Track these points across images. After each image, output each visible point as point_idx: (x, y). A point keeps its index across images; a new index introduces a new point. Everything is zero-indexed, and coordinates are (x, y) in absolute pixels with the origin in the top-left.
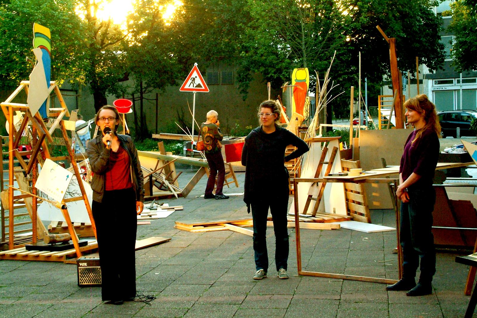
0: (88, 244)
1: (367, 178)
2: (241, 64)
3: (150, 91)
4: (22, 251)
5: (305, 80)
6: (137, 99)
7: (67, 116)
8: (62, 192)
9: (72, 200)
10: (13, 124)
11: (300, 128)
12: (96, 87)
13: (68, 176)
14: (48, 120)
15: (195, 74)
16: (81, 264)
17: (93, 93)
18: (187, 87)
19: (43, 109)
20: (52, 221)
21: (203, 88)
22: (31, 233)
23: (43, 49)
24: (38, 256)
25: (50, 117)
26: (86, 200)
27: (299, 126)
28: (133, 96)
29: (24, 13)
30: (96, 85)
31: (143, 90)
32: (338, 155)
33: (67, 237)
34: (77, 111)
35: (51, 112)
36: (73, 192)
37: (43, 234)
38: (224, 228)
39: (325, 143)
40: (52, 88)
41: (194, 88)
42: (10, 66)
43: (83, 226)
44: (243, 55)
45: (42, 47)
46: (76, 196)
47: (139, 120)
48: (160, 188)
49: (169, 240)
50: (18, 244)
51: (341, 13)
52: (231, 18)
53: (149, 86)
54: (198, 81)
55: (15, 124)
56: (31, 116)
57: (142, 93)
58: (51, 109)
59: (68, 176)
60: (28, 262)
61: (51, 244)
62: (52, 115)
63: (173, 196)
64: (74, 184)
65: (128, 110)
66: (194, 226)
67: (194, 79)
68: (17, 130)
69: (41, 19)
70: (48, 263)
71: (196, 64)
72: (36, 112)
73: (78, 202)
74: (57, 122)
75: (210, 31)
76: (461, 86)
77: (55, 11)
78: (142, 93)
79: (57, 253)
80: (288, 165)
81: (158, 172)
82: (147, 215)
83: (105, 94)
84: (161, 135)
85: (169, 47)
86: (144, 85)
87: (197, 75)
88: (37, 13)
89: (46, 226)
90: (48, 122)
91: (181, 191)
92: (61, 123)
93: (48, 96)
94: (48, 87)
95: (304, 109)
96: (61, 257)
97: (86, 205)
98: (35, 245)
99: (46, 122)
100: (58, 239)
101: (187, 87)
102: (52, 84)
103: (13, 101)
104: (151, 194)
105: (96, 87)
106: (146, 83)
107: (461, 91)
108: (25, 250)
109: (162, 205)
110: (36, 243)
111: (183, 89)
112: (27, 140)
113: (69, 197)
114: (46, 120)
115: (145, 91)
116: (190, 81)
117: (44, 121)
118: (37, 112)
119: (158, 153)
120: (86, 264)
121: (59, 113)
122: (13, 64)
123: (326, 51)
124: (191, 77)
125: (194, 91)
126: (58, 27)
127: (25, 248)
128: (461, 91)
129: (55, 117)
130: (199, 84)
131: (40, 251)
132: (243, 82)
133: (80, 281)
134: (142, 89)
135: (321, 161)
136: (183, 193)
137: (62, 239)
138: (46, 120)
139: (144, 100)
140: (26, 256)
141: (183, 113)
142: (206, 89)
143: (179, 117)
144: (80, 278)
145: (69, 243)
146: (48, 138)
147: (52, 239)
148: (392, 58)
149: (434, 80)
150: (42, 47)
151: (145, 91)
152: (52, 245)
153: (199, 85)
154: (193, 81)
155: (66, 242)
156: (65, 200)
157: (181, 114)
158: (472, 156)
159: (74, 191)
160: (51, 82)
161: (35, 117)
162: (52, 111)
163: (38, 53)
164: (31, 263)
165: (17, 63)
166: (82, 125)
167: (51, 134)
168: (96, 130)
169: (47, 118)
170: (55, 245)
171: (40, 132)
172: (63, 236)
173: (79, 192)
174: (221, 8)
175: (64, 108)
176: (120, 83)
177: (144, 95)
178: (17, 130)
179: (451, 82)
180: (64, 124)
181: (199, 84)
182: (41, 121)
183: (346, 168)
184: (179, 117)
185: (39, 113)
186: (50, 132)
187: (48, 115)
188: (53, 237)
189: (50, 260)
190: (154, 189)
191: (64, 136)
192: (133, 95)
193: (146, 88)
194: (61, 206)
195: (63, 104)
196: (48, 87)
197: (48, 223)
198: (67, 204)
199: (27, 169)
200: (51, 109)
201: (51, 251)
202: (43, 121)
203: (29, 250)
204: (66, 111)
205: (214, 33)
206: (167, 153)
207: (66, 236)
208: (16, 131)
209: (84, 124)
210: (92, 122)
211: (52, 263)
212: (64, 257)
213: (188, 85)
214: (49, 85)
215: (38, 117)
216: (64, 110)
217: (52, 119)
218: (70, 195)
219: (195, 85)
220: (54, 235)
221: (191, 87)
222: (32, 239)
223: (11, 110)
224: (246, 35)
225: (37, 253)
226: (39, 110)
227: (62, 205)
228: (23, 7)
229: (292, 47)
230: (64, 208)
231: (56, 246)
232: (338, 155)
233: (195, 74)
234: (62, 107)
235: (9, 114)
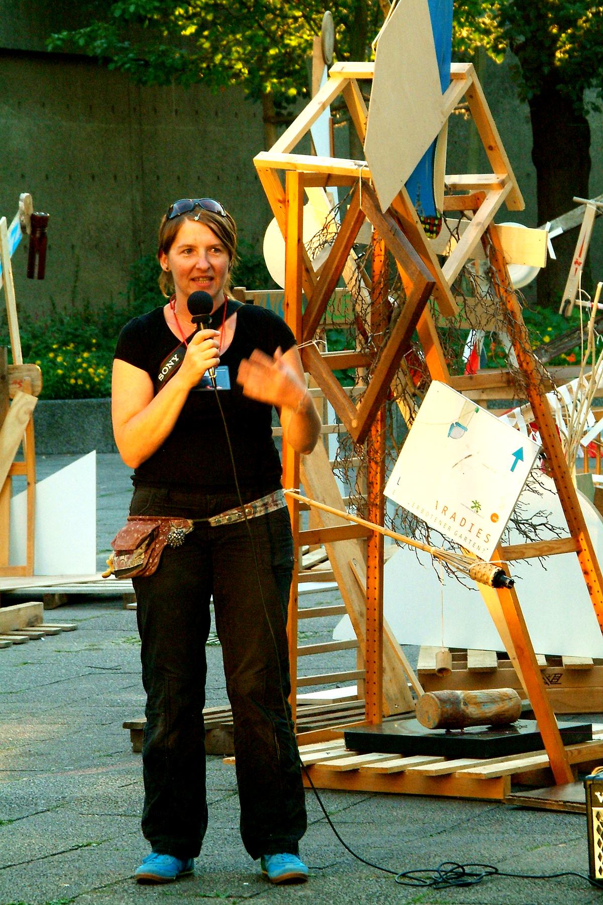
0: (594, 737)
4: (333, 753)
7: (511, 208)
9: (532, 552)
10: (300, 240)
12: (546, 70)
13: (519, 455)
14: (439, 226)
17: (530, 95)
20: (424, 644)
22: (351, 690)
24: (398, 775)
25: (447, 214)
26: (586, 554)
30: (544, 59)
33: (508, 705)
35: (451, 190)
36: (536, 521)
37: (401, 691)
40: (458, 90)
43: (557, 669)
46: (546, 535)
50: (308, 729)
55: (306, 240)
56: (378, 207)
59: (519, 455)
60: (357, 799)
61: (443, 731)
62: (454, 203)
64: (537, 487)
68: (316, 267)
70: (443, 805)
72: (396, 194)
73: (552, 561)
74: (472, 233)
79: (474, 766)
80: (305, 765)
83: (580, 99)
89: (413, 659)
90: (437, 233)
92: (488, 239)
93: (442, 131)
94: (444, 88)
96: (495, 779)
97: (586, 573)
98: (375, 731)
99: (432, 232)
102: (459, 76)
105: (546, 70)
108: (343, 751)
110: (379, 726)
112: (351, 308)
113: (517, 539)
117: (426, 230)
118: (400, 194)
127: (342, 742)
131: (405, 754)
137: (491, 710)
138: (432, 225)
140: (353, 773)
145: (514, 729)
146: (441, 299)
147: (448, 707)
152: (448, 732)
156: (505, 552)
159: (539, 514)
161: (391, 212)
162: (454, 186)
164: (374, 802)
167: (450, 284)
168: (582, 260)
169: (436, 218)
170: (463, 734)
171: (411, 275)
172: (493, 701)
173: (559, 519)
175: (503, 176)
178: (316, 267)
180: (498, 239)
182: (416, 230)
186: (449, 273)
187: (441, 202)
188: (455, 702)
189: (449, 790)
194: (491, 576)
195: (500, 156)
196: (444, 88)
197: (413, 651)
198: (516, 569)
199: (354, 424)
201: (449, 758)
202: (420, 227)
203: (361, 752)
204: (508, 187)
207: (503, 698)
208: (308, 270)
210: (559, 231)
211: (455, 805)
212: (502, 780)
214: (447, 80)
215: (400, 210)
216: (502, 184)
217: (452, 222)
218: (519, 529)
220: (459, 692)
222: (363, 710)
225: (394, 762)
226: (405, 185)
227: (495, 570)
230: (501, 581)
231: (465, 737)
234: (492, 172)
235: (285, 202)
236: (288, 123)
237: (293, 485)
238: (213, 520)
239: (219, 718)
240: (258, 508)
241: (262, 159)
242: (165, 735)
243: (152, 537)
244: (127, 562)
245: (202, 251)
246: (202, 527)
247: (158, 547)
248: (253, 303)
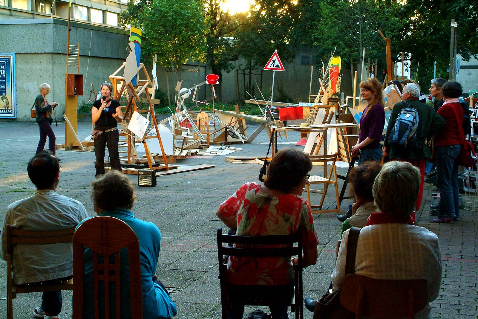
1: (310, 129)
2: (318, 50)
3: (257, 69)
5: (338, 65)
6: (247, 74)
8: (143, 132)
10: (116, 89)
11: (330, 99)
13: (146, 123)
15: (275, 58)
16: (140, 173)
18: (269, 67)
19: (134, 80)
21: (280, 68)
23: (136, 43)
24: (133, 171)
27: (330, 97)
28: (244, 72)
29: (161, 11)
31: (252, 68)
32: (334, 117)
34: (182, 82)
35: (139, 82)
38: (255, 162)
40: (140, 67)
41: (274, 68)
42: (150, 48)
44: (316, 44)
45: (135, 42)
48: (233, 137)
49: (214, 166)
52: (312, 16)
53: (256, 64)
54: (277, 63)
57: (251, 70)
58: (140, 80)
59: (146, 123)
63: (241, 143)
65: (216, 82)
66: (235, 160)
67: (274, 61)
69: (173, 15)
71: (276, 51)
75: (298, 25)
77: (183, 10)
78: (251, 70)
81: (233, 125)
82: (215, 153)
84: (251, 101)
85: (267, 36)
86: (253, 64)
88: (169, 11)
91: (247, 139)
92: (146, 89)
95: (337, 85)
100: (141, 162)
101: (269, 67)
104: (226, 140)
106: (254, 62)
109: (229, 147)
111: (266, 68)
114: (136, 87)
115: (253, 68)
116: (271, 63)
119: (235, 113)
120: (143, 173)
121: (145, 83)
122: (153, 47)
123: (377, 43)
125: (274, 70)
126: (184, 21)
129: (142, 86)
130: (278, 65)
132: (319, 64)
133: (139, 183)
134: (251, 67)
135: (324, 121)
136: (249, 141)
137: (144, 162)
139: (252, 74)
141: (282, 86)
142: (282, 69)
143: (279, 88)
144: (139, 181)
147: (137, 161)
148: (387, 52)
150: (135, 42)
151: (253, 68)
153: (277, 66)
155: (146, 163)
157: (280, 86)
158: (355, 116)
160: (141, 64)
163: (132, 45)
165: (156, 46)
166: (185, 91)
174: (306, 9)
176: (230, 62)
177: (252, 71)
181: (278, 65)
184: (279, 88)
185: (131, 82)
190: (229, 137)
191: (148, 97)
192: (244, 71)
193: (254, 66)
204: (149, 82)
205: (300, 27)
206: (241, 112)
209: (187, 91)
210: (192, 90)
213: (270, 66)
214: (138, 65)
216: (149, 81)
219: (275, 66)
221: (272, 67)
223: (115, 80)
228: (161, 7)
229: (209, 54)
230: (144, 142)
232: (334, 117)
233: (275, 58)
235: (114, 83)
236: (450, 44)
237: (360, 238)
238: (106, 131)
239: (11, 77)
240: (113, 129)
241: (110, 76)
242: (50, 116)
243: (96, 133)
244: (93, 137)
245: (105, 90)
246: (104, 132)
247: (97, 135)
248: (302, 134)
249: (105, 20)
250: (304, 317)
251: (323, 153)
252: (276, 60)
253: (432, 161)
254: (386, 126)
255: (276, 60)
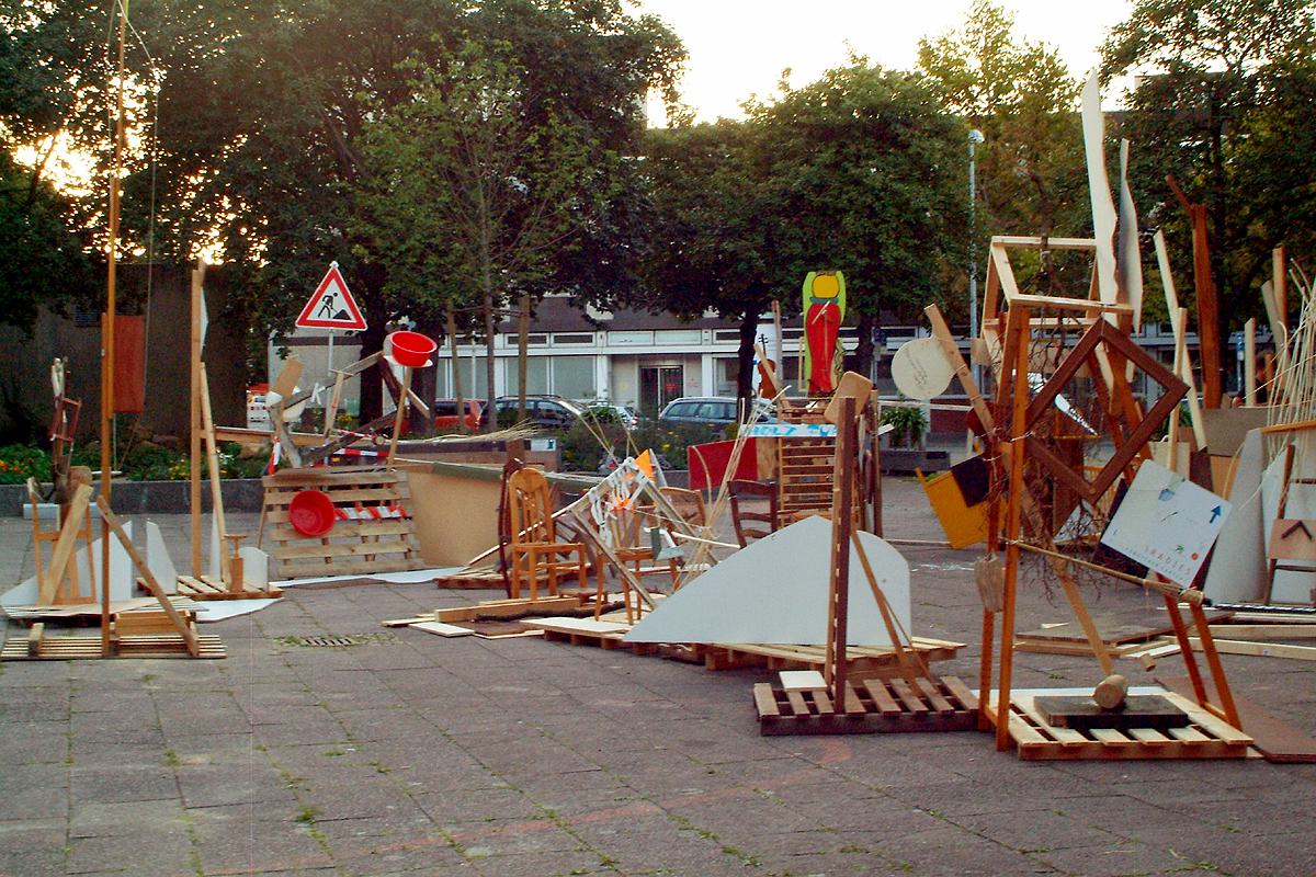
15: (333, 288)
21: (354, 320)
39: (746, 525)
47: (284, 485)
51: (86, 237)
54: (340, 304)
67: (330, 299)
76: (474, 350)
87: (338, 290)
103: (349, 319)
107: (474, 360)
116: (321, 304)
124: (325, 294)
128: (474, 360)
139: (643, 613)
149: (507, 335)
153: (343, 315)
154: (327, 303)
179: (543, 340)
183: (795, 690)
200: (474, 395)
219: (333, 314)
224: (845, 234)
233: (333, 288)
239: (1258, 611)
249: (1125, 246)
250: (1314, 635)
251: (887, 445)
252: (336, 295)
253: (624, 117)
254: (910, 695)
255: (336, 295)
